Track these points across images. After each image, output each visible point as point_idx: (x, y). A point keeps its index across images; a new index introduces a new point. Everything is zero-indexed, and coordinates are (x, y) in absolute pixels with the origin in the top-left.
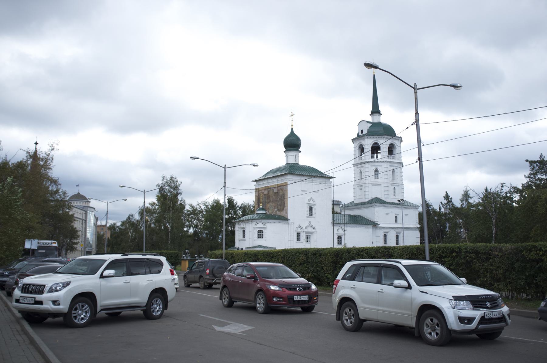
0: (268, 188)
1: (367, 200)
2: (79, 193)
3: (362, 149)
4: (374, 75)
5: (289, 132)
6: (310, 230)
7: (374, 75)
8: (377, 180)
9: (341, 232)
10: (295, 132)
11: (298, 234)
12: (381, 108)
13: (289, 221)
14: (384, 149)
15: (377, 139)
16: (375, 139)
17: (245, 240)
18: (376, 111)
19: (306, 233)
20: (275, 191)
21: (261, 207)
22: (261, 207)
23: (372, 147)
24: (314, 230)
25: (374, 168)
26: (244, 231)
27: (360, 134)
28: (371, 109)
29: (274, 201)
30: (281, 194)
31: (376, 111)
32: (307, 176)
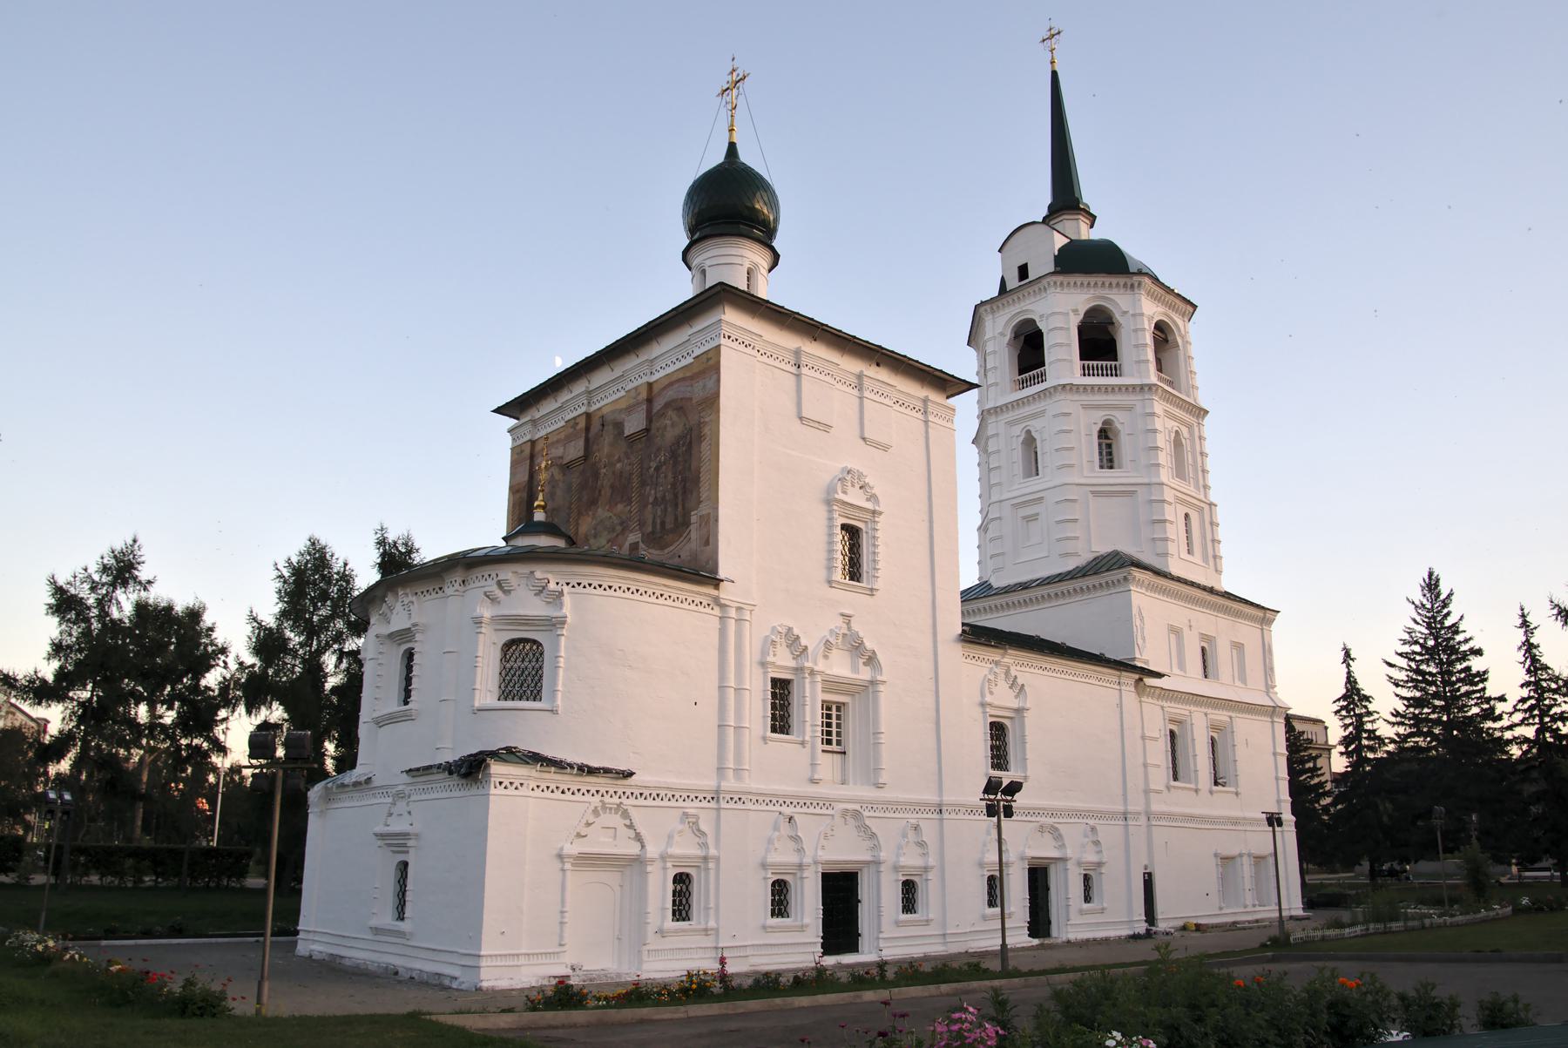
0: (590, 428)
1: (1070, 565)
2: (194, 615)
3: (1029, 349)
4: (1054, 75)
5: (717, 157)
6: (840, 666)
7: (1054, 75)
8: (400, 923)
9: (1003, 698)
10: (746, 157)
11: (781, 691)
12: (1089, 193)
13: (726, 593)
14: (1135, 344)
15: (1105, 292)
16: (1100, 292)
17: (406, 717)
18: (1066, 198)
19: (832, 684)
20: (634, 424)
21: (539, 516)
22: (539, 516)
23: (1082, 329)
24: (865, 674)
25: (1098, 418)
26: (409, 656)
27: (1013, 282)
28: (1048, 200)
29: (621, 491)
30: (671, 434)
31: (1066, 198)
32: (556, 1027)
